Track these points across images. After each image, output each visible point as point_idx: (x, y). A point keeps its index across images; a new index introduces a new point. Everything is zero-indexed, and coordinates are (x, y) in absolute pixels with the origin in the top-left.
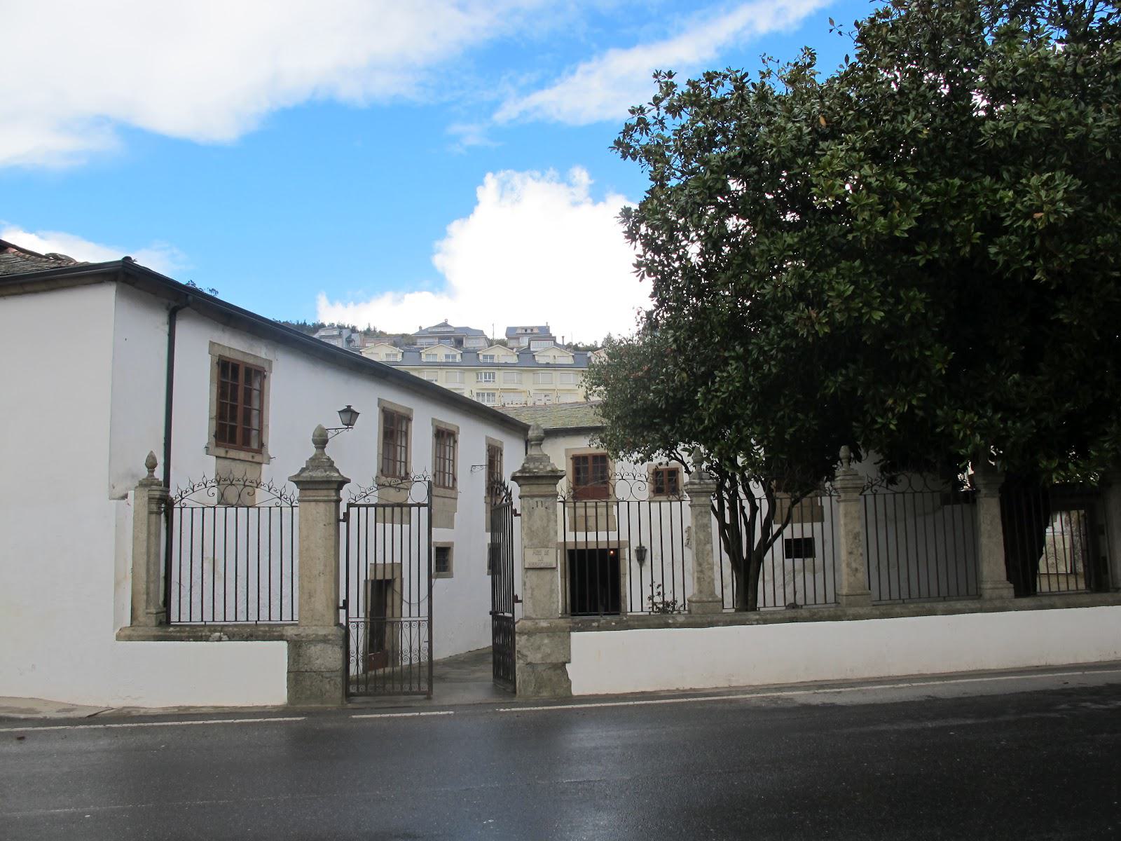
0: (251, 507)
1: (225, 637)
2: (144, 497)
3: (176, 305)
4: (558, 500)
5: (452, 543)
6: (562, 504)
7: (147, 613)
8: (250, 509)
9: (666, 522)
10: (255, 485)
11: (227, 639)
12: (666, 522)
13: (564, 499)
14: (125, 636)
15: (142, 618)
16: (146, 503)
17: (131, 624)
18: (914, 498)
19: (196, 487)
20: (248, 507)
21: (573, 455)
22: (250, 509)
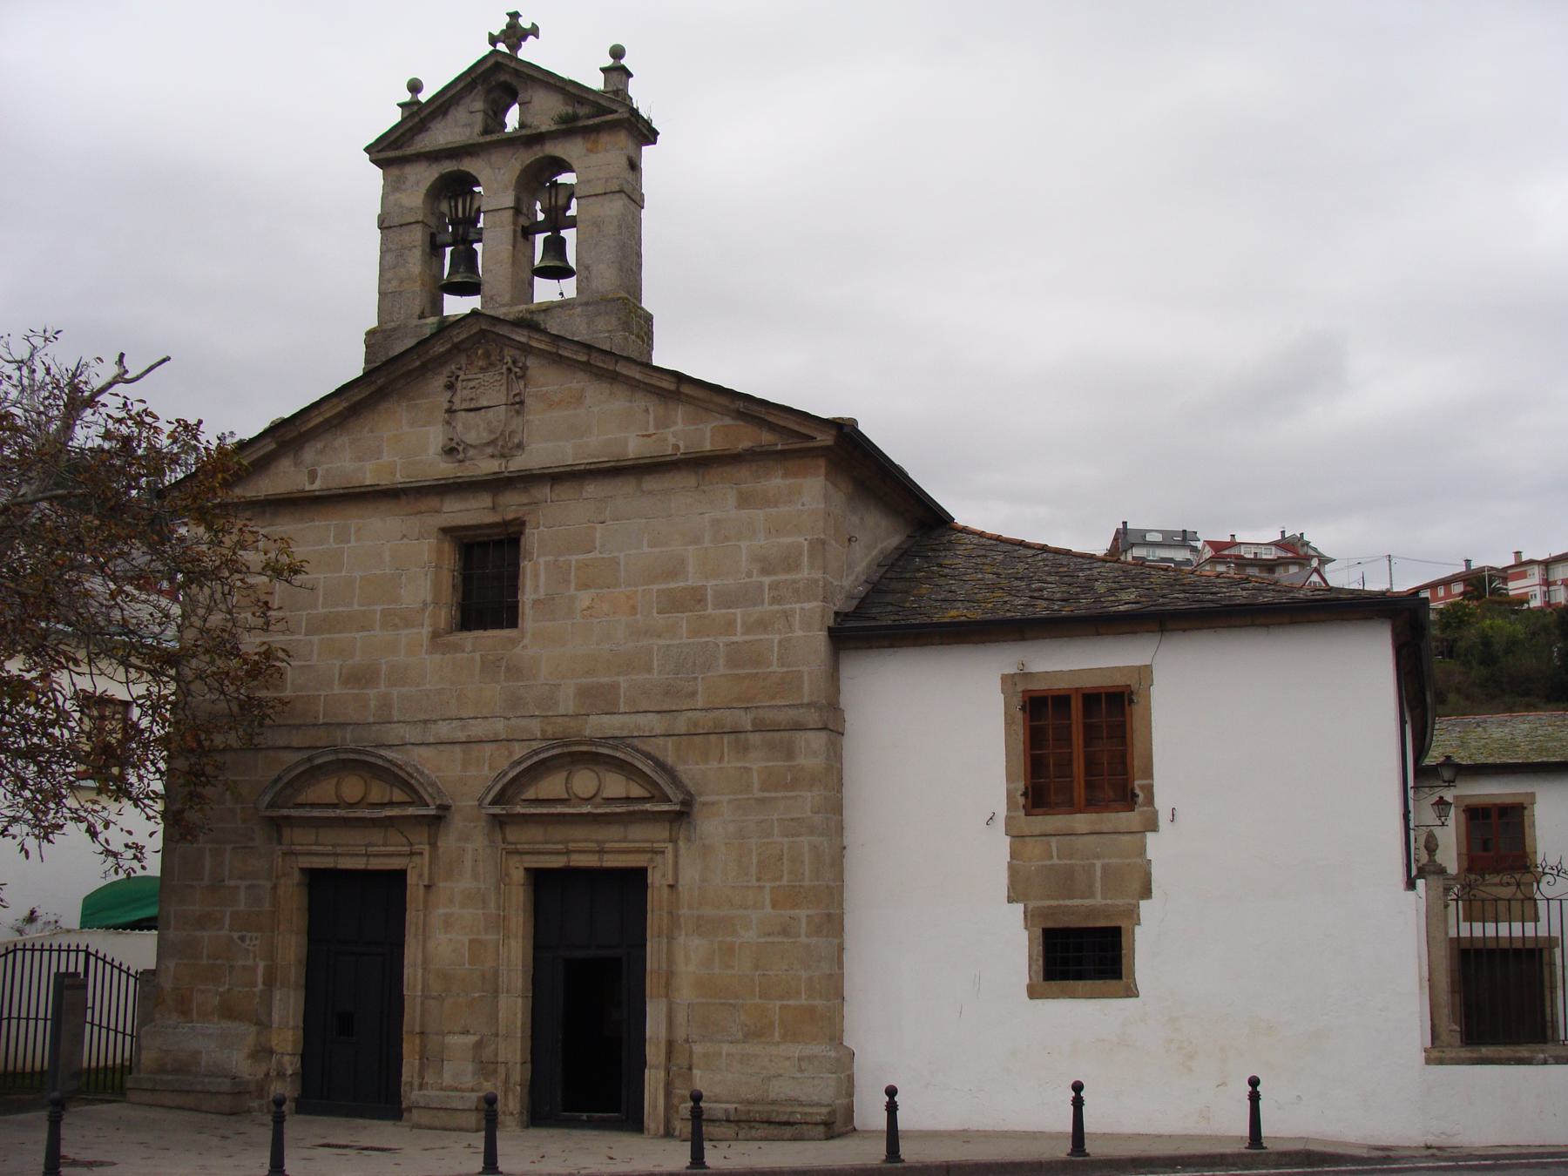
0: (1552, 899)
1: (1551, 1060)
2: (1438, 887)
3: (1189, 557)
4: (1449, 898)
5: (1033, 993)
6: (1455, 902)
7: (1451, 1031)
8: (1550, 901)
9: (31, 1036)
10: (1555, 872)
11: (1553, 1062)
12: (31, 1036)
13: (1457, 896)
14: (1436, 1058)
15: (1444, 1037)
16: (1442, 894)
17: (1433, 1043)
18: (1523, 906)
19: (1547, 868)
20: (1496, 901)
21: (1466, 806)
22: (1550, 901)
